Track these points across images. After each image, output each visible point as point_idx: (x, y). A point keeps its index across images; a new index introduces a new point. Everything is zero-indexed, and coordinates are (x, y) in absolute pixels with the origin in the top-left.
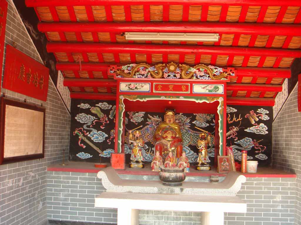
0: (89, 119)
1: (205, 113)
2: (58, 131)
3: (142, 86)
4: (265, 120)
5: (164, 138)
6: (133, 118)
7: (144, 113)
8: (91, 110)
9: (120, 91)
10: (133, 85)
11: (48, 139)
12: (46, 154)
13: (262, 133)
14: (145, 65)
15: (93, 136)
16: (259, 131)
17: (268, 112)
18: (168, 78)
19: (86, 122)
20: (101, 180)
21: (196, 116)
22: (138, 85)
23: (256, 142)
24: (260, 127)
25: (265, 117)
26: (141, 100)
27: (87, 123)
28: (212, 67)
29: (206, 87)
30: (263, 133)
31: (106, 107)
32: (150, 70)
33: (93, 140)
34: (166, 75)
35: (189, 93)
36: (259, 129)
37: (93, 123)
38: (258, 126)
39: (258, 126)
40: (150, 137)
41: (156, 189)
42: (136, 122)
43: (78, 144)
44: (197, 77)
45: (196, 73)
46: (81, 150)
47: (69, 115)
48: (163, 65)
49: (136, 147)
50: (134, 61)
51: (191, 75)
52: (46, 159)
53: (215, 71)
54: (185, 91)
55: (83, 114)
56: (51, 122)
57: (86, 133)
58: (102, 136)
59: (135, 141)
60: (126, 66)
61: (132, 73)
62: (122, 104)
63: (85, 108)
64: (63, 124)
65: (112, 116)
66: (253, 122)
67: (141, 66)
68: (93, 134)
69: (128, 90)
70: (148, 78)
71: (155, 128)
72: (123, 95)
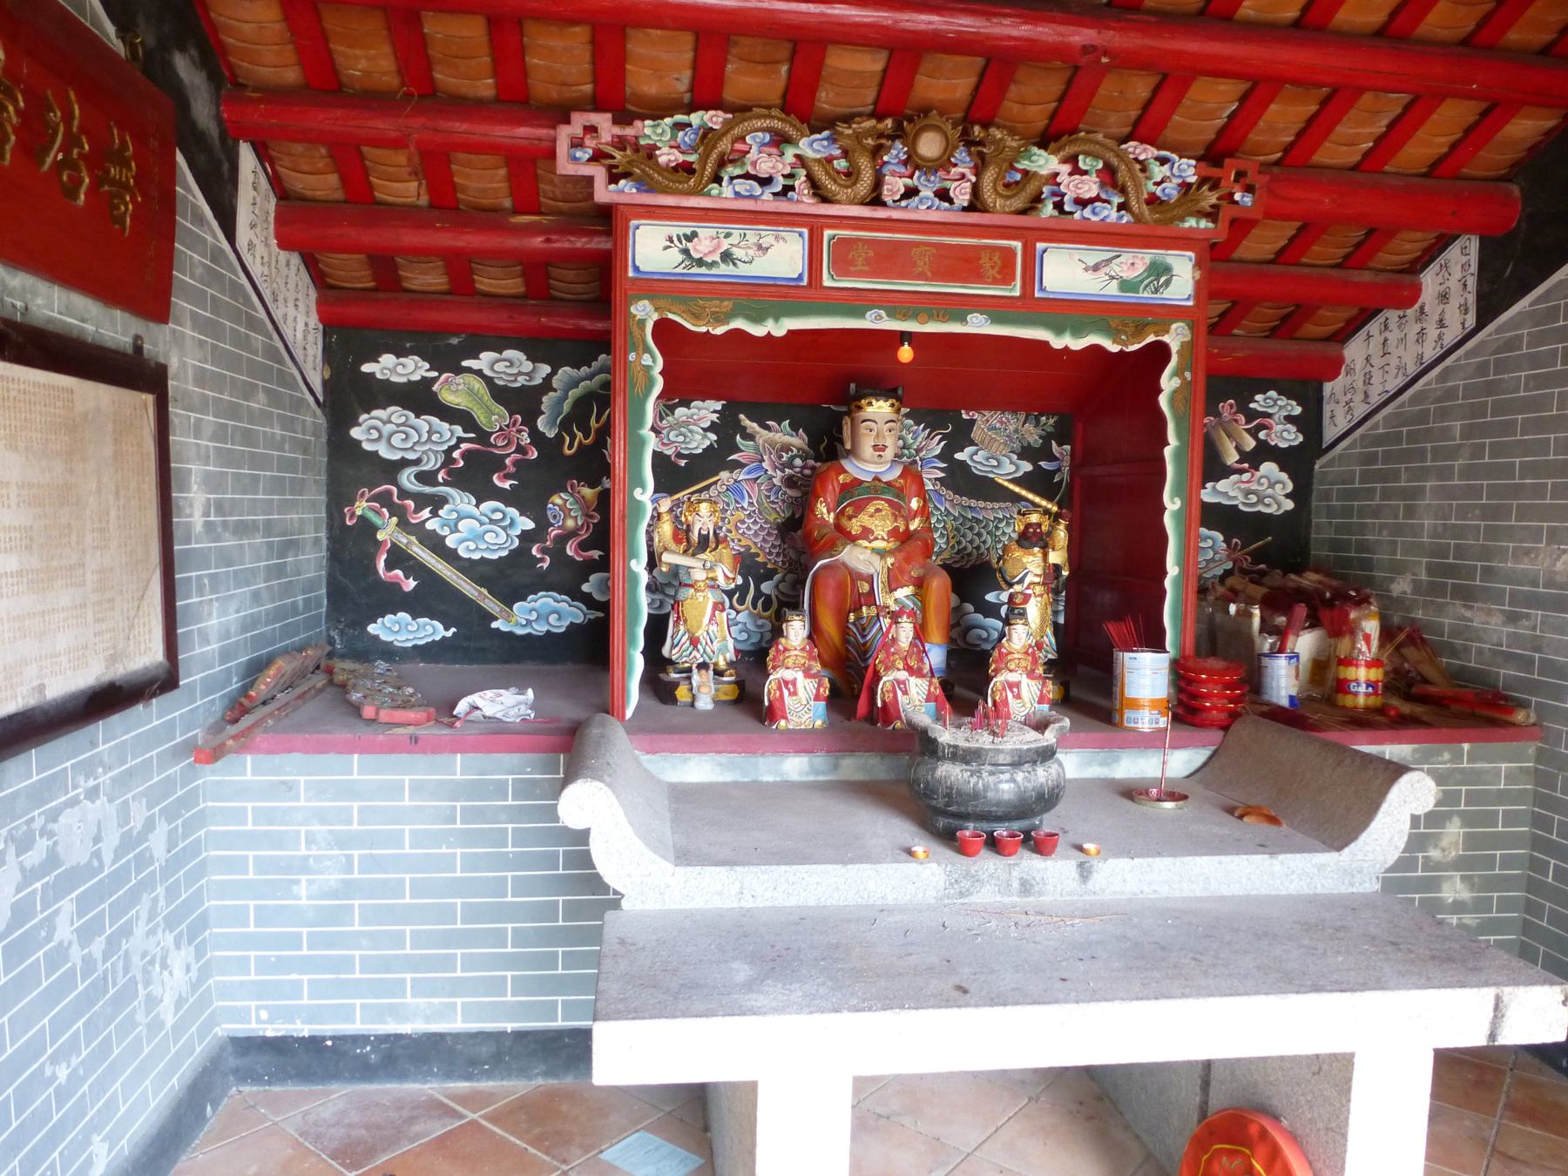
0: (429, 439)
1: (1014, 410)
2: (254, 507)
3: (760, 247)
4: (1283, 445)
5: (852, 539)
6: (664, 432)
7: (718, 406)
8: (435, 388)
9: (631, 274)
10: (708, 239)
11: (202, 559)
13: (1268, 505)
14: (779, 119)
15: (455, 530)
16: (1254, 499)
17: (1298, 410)
18: (903, 203)
19: (411, 456)
20: (583, 836)
21: (972, 422)
22: (741, 239)
23: (1242, 549)
24: (1263, 480)
25: (1285, 434)
26: (758, 331)
27: (417, 462)
28: (1147, 152)
29: (1109, 261)
30: (1272, 510)
31: (520, 373)
32: (809, 153)
33: (456, 550)
34: (894, 185)
35: (1017, 293)
36: (1254, 487)
37: (454, 461)
38: (1253, 475)
39: (1253, 475)
40: (749, 528)
41: (933, 875)
42: (679, 455)
43: (377, 572)
44: (1059, 206)
45: (1059, 185)
46: (392, 600)
47: (315, 416)
48: (881, 126)
49: (697, 591)
50: (705, 94)
51: (1031, 188)
52: (191, 686)
53: (1158, 172)
54: (995, 282)
55: (396, 413)
56: (287, 447)
57: (418, 509)
58: (504, 528)
59: (693, 555)
60: (668, 121)
61: (704, 169)
62: (647, 350)
63: (403, 380)
64: (289, 465)
65: (552, 423)
66: (1232, 458)
67: (759, 123)
68: (455, 515)
69: (679, 270)
70: (791, 200)
71: (776, 481)
72: (651, 300)
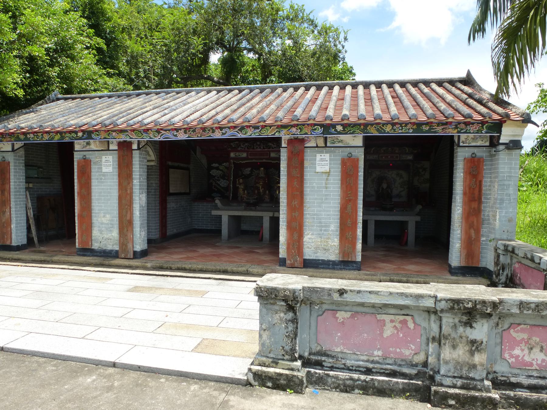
10: (237, 154)
12: (432, 293)
34: (255, 147)
